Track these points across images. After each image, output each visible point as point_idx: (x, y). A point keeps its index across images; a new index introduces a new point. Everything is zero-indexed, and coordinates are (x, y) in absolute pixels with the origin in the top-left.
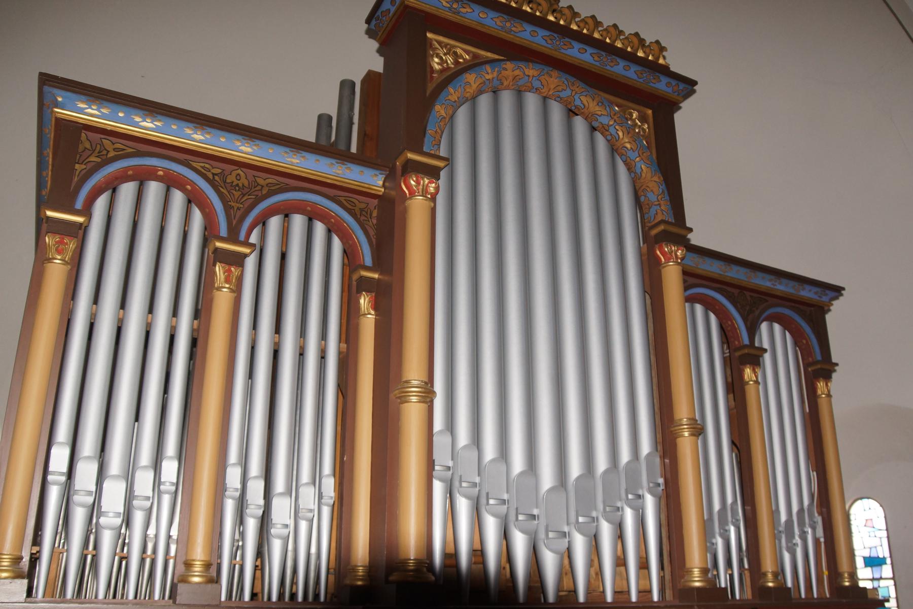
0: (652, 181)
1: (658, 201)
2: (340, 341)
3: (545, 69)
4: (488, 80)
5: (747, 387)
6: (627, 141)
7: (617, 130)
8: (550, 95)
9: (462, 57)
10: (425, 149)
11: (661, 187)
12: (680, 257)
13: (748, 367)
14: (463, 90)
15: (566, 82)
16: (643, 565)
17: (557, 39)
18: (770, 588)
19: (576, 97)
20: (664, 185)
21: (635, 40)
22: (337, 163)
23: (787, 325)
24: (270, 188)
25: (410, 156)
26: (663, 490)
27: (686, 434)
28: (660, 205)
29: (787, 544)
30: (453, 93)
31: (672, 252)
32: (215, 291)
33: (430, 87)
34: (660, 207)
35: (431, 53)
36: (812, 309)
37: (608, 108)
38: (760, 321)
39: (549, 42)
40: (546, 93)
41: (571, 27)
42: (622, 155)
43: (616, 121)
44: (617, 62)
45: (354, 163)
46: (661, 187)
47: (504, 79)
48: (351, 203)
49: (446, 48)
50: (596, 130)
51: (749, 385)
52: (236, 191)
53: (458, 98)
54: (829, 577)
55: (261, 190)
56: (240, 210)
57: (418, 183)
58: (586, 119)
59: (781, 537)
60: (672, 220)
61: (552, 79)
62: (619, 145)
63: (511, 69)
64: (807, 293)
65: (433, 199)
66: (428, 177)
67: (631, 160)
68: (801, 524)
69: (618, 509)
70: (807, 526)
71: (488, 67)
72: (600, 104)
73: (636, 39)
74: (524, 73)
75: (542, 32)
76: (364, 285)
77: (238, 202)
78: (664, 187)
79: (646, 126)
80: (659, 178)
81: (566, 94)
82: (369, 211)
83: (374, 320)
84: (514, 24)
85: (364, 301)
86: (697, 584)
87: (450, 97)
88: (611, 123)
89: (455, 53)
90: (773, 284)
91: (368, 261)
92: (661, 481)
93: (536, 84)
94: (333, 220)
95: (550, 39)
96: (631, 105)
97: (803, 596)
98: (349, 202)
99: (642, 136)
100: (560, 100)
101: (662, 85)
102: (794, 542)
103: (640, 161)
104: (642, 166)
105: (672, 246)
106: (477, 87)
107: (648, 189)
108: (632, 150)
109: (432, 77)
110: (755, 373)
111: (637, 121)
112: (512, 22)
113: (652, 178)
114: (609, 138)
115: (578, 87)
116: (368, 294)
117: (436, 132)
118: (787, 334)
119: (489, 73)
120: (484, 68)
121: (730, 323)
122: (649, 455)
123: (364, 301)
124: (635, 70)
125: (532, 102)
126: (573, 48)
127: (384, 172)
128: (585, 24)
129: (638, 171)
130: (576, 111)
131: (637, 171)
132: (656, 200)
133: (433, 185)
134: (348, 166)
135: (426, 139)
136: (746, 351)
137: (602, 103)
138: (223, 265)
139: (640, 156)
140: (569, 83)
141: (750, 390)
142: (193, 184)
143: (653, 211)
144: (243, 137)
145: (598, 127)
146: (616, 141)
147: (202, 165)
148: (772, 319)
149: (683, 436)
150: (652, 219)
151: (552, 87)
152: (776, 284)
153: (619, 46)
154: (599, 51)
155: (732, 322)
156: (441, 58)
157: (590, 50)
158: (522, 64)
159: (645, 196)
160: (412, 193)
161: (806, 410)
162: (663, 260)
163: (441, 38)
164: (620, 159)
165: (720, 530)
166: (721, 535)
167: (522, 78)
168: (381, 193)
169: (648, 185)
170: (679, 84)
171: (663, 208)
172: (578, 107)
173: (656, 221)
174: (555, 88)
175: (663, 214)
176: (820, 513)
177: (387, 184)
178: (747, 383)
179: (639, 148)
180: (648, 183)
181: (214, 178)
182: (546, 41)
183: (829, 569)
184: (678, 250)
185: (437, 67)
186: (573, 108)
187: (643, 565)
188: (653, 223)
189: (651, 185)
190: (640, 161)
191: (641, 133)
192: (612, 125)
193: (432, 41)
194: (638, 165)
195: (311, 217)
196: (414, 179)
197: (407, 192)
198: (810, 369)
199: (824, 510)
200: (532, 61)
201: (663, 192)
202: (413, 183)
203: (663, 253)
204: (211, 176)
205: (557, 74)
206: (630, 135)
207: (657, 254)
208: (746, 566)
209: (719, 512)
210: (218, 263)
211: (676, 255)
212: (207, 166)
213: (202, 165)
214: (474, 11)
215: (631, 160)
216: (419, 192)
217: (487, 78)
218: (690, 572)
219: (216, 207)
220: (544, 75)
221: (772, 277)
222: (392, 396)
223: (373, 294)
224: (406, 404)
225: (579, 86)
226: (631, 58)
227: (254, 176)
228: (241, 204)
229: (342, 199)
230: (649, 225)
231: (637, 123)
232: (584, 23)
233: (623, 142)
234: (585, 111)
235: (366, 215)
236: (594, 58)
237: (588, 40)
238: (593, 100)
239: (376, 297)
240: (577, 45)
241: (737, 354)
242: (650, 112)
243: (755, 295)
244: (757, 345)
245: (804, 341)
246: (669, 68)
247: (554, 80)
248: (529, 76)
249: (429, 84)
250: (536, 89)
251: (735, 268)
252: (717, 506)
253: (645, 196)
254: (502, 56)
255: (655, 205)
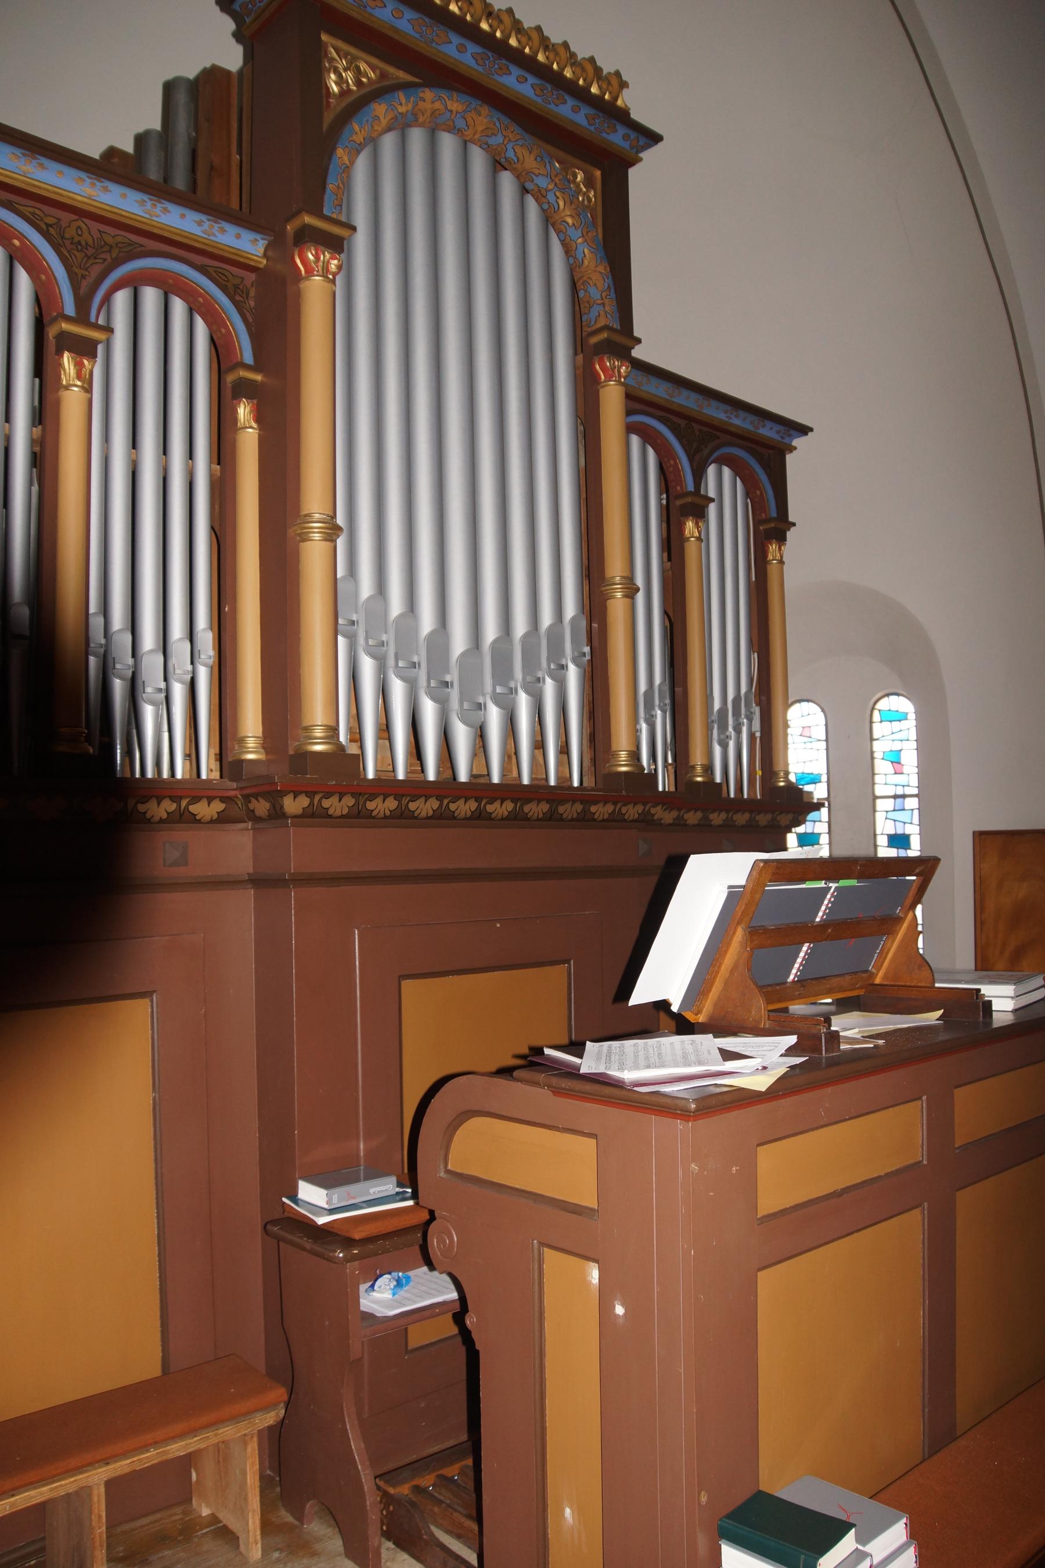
0: (595, 271)
1: (602, 299)
2: (211, 462)
3: (473, 102)
4: (400, 113)
5: (687, 545)
6: (569, 214)
7: (558, 198)
8: (475, 139)
9: (366, 76)
10: (326, 212)
11: (606, 280)
12: (624, 374)
13: (690, 520)
14: (371, 127)
15: (498, 124)
16: (564, 750)
17: (491, 59)
18: (699, 783)
19: (509, 147)
20: (610, 277)
21: (590, 69)
22: (24, 155)
23: (739, 470)
24: (123, 250)
25: (308, 219)
26: (588, 660)
27: (619, 595)
28: (603, 304)
29: (719, 735)
30: (357, 130)
31: (615, 367)
32: (62, 390)
33: (328, 118)
34: (604, 307)
35: (327, 65)
36: (771, 451)
37: (548, 166)
38: (708, 464)
39: (481, 62)
40: (470, 136)
41: (510, 42)
42: (560, 232)
43: (558, 184)
44: (565, 99)
45: (230, 222)
46: (606, 280)
47: (421, 114)
48: (223, 277)
49: (346, 59)
50: (528, 193)
51: (689, 542)
52: (78, 251)
53: (364, 139)
54: (762, 778)
55: (110, 251)
56: (85, 278)
57: (317, 258)
58: (517, 178)
59: (713, 728)
60: (617, 326)
61: (481, 118)
62: (557, 218)
63: (430, 99)
64: (768, 432)
65: (333, 282)
66: (330, 251)
67: (571, 240)
68: (737, 713)
69: (538, 680)
70: (743, 716)
71: (401, 95)
72: (539, 159)
73: (591, 67)
74: (446, 107)
75: (472, 48)
76: (244, 390)
77: (82, 267)
78: (610, 281)
79: (592, 194)
80: (605, 267)
81: (496, 140)
82: (245, 288)
83: (257, 435)
84: (437, 32)
85: (244, 411)
86: (624, 769)
87: (355, 137)
88: (551, 187)
89: (358, 68)
90: (727, 417)
91: (248, 358)
92: (587, 649)
93: (460, 123)
94: (201, 299)
95: (482, 59)
96: (576, 161)
97: (732, 795)
98: (220, 275)
99: (587, 207)
100: (486, 147)
101: (618, 138)
102: (728, 734)
103: (584, 242)
104: (586, 250)
105: (615, 360)
106: (387, 123)
107: (590, 282)
108: (573, 227)
109: (328, 103)
110: (698, 527)
111: (582, 186)
112: (435, 29)
113: (596, 267)
114: (546, 207)
115: (512, 132)
116: (249, 401)
117: (338, 187)
118: (738, 479)
119: (403, 104)
120: (396, 95)
121: (672, 462)
122: (573, 619)
123: (244, 411)
124: (585, 112)
125: (448, 143)
126: (511, 74)
127: (266, 237)
128: (528, 40)
129: (580, 256)
130: (506, 165)
131: (578, 256)
132: (600, 298)
133: (336, 262)
134: (222, 226)
135: (326, 197)
136: (689, 499)
137: (542, 159)
138: (73, 355)
139: (583, 236)
140: (502, 125)
141: (691, 549)
142: (22, 237)
143: (595, 311)
144: (89, 175)
145: (533, 190)
146: (555, 212)
147: (31, 210)
148: (722, 461)
149: (613, 597)
150: (592, 323)
151: (480, 129)
152: (732, 416)
153: (568, 75)
154: (543, 82)
155: (675, 462)
156: (340, 76)
157: (532, 80)
158: (444, 94)
159: (586, 291)
160: (310, 272)
161: (752, 579)
162: (603, 377)
163: (340, 44)
164: (552, 229)
165: (645, 715)
166: (647, 721)
167: (443, 114)
168: (261, 266)
169: (590, 276)
170: (640, 138)
171: (607, 308)
172: (510, 159)
173: (598, 326)
174: (483, 130)
175: (607, 317)
176: (759, 704)
177: (270, 253)
178: (688, 539)
179: (582, 226)
180: (590, 273)
181: (48, 230)
182: (476, 60)
183: (762, 769)
184: (622, 365)
185: (335, 88)
186: (503, 160)
187: (564, 750)
188: (593, 328)
189: (595, 277)
190: (584, 242)
191: (586, 202)
192: (551, 190)
193: (327, 47)
194: (580, 249)
195: (166, 291)
196: (313, 252)
197: (302, 269)
198: (761, 528)
199: (763, 698)
200: (457, 90)
201: (609, 287)
202: (311, 257)
203: (604, 369)
204: (44, 227)
205: (487, 111)
206: (573, 206)
207: (595, 369)
208: (670, 761)
209: (645, 693)
210: (66, 352)
211: (619, 372)
212: (37, 212)
213: (31, 210)
214: (385, 6)
215: (571, 240)
216: (318, 271)
217: (400, 111)
218: (615, 755)
219: (57, 274)
220: (471, 112)
221: (729, 408)
222: (291, 532)
223: (255, 401)
224: (309, 542)
225: (514, 130)
226: (582, 95)
227: (100, 231)
228: (86, 270)
229: (211, 270)
230: (589, 330)
231: (581, 190)
232: (527, 37)
233: (563, 214)
234: (518, 166)
235: (241, 294)
236: (535, 90)
237: (528, 64)
238: (530, 153)
239: (258, 405)
240: (516, 71)
241: (678, 503)
242: (598, 173)
243: (704, 429)
244: (702, 492)
245: (758, 492)
246: (629, 114)
247: (484, 117)
248: (451, 111)
249: (326, 113)
250: (458, 130)
251: (685, 393)
252: (643, 687)
253: (586, 291)
254: (417, 77)
255: (597, 304)
